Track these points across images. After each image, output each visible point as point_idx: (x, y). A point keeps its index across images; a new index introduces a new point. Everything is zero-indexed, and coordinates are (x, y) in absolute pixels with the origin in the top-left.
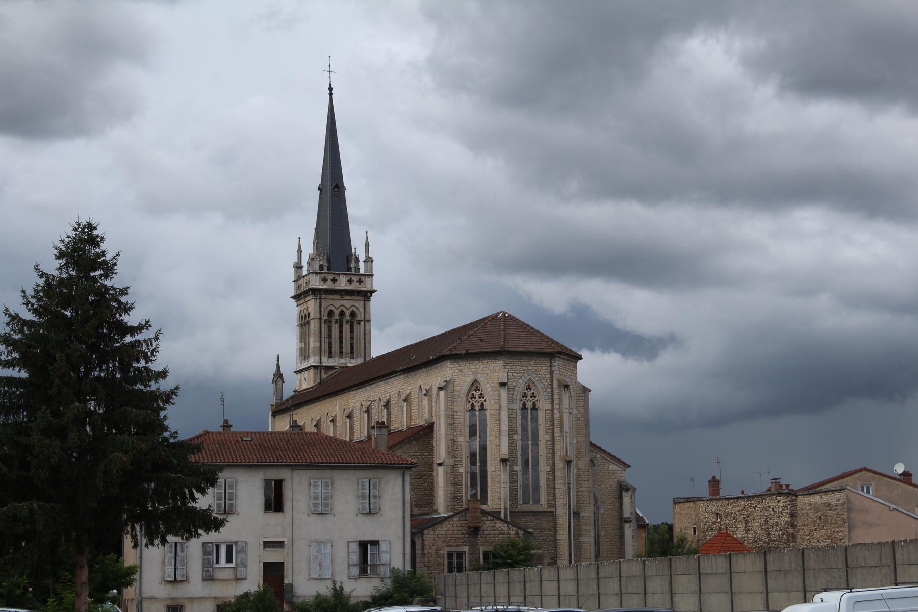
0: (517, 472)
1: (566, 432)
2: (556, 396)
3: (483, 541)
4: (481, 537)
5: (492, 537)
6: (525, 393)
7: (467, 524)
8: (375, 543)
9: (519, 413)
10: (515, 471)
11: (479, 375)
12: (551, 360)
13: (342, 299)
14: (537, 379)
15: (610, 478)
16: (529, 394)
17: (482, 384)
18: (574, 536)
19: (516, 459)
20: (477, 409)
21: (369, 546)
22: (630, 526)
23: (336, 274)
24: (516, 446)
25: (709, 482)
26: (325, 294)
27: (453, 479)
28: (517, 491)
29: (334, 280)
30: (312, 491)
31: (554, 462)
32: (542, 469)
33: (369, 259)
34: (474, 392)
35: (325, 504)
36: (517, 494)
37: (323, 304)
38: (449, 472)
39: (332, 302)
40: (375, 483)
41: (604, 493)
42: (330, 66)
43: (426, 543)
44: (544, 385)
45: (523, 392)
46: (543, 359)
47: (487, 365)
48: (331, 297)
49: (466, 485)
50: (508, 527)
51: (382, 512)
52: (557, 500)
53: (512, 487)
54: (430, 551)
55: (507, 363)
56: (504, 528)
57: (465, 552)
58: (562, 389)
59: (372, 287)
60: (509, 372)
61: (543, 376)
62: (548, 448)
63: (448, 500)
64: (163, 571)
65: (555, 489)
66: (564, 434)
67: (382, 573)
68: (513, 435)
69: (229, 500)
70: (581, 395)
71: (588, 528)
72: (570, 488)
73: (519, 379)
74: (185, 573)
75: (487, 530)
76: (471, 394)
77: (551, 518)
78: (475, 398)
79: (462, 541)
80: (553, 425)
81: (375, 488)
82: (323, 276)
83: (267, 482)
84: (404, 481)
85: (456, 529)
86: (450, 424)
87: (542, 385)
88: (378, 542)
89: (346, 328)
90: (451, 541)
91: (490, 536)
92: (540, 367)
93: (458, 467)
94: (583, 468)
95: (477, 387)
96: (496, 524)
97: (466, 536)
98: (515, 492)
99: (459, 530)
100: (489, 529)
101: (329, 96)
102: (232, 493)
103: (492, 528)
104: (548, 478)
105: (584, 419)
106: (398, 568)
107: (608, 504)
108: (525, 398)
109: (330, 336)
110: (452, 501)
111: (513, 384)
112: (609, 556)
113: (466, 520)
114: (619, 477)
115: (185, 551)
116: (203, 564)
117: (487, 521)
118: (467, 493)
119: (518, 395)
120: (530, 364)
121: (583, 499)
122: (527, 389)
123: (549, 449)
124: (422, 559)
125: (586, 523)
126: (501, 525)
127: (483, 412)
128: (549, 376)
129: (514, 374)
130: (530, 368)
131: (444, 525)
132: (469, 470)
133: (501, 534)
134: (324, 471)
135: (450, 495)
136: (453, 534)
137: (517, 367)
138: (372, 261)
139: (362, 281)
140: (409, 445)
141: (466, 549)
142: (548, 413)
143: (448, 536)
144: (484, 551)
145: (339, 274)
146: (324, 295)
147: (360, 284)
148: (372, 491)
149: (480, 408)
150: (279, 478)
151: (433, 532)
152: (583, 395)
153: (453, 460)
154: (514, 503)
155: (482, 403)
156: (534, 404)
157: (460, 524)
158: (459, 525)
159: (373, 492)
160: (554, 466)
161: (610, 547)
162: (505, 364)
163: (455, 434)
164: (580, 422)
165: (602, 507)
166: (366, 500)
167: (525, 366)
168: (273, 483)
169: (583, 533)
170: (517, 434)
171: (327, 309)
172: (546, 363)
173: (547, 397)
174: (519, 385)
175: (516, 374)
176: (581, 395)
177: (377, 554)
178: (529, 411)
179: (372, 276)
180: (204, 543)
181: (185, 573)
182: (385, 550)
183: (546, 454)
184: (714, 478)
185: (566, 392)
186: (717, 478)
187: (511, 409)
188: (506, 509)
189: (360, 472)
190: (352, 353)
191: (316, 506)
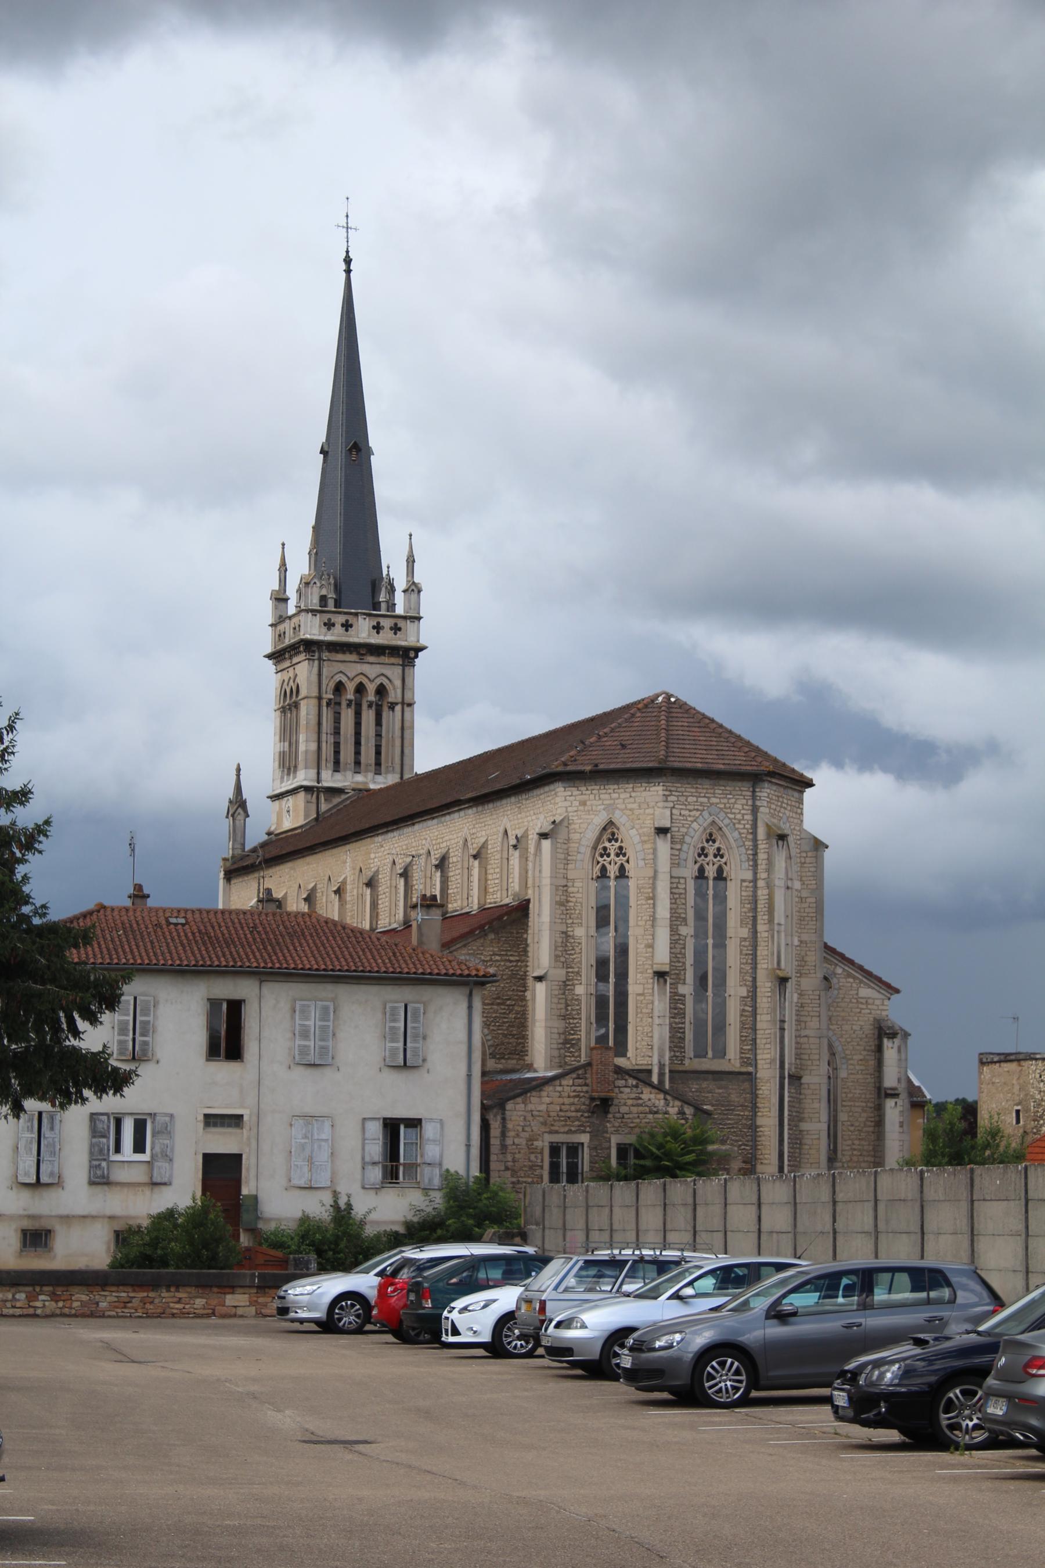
0: (684, 996)
1: (779, 924)
2: (762, 856)
3: (617, 1124)
4: (614, 1117)
5: (635, 1118)
6: (616, 840)
7: (587, 1092)
8: (415, 1123)
10: (681, 995)
11: (617, 812)
13: (361, 661)
14: (727, 821)
15: (860, 1012)
16: (711, 849)
17: (622, 828)
19: (682, 973)
20: (612, 876)
21: (402, 1127)
22: (896, 1103)
23: (351, 614)
24: (684, 948)
26: (330, 651)
28: (684, 1033)
29: (347, 626)
30: (298, 1022)
31: (754, 979)
32: (732, 993)
33: (413, 587)
34: (607, 844)
35: (322, 1047)
36: (684, 1039)
37: (325, 671)
39: (342, 667)
40: (416, 1011)
41: (849, 1040)
42: (347, 216)
43: (510, 1125)
44: (740, 834)
46: (740, 784)
47: (633, 794)
48: (340, 657)
49: (588, 1018)
50: (665, 1099)
51: (428, 1065)
52: (758, 1051)
53: (674, 1025)
55: (670, 791)
56: (657, 1102)
57: (582, 1144)
58: (775, 841)
59: (418, 641)
60: (674, 807)
61: (739, 816)
62: (744, 952)
63: (552, 1046)
64: (16, 1163)
66: (776, 928)
68: (680, 927)
69: (143, 1035)
72: (784, 1029)
73: (692, 822)
74: (56, 1170)
75: (625, 1104)
76: (600, 847)
77: (746, 1085)
78: (608, 855)
79: (577, 1123)
80: (755, 909)
81: (416, 1020)
82: (326, 617)
83: (214, 1004)
84: (470, 1007)
85: (567, 1101)
87: (736, 834)
89: (368, 717)
90: (556, 1123)
91: (631, 1116)
92: (733, 801)
93: (573, 985)
94: (811, 992)
95: (613, 834)
96: (642, 1093)
97: (586, 1115)
98: (679, 1035)
99: (573, 1104)
100: (630, 1102)
101: (344, 275)
102: (149, 1022)
103: (635, 1102)
104: (744, 1010)
105: (813, 900)
106: (456, 1172)
107: (855, 1062)
109: (337, 732)
110: (559, 1049)
111: (682, 830)
112: (855, 1159)
113: (586, 1085)
114: (878, 1012)
115: (57, 1127)
116: (91, 1153)
117: (626, 1087)
118: (588, 1033)
119: (690, 852)
120: (714, 793)
121: (809, 1051)
123: (746, 955)
124: (501, 1156)
125: (814, 1097)
126: (652, 1096)
127: (623, 881)
128: (749, 817)
129: (683, 812)
130: (714, 800)
131: (544, 1094)
132: (593, 991)
133: (651, 1112)
134: (321, 986)
135: (556, 1036)
137: (690, 799)
138: (419, 591)
139: (400, 629)
140: (482, 941)
141: (584, 1138)
142: (747, 887)
143: (552, 1114)
144: (618, 1144)
145: (356, 614)
146: (327, 654)
147: (395, 634)
149: (716, 875)
150: (236, 996)
151: (523, 1106)
153: (563, 972)
154: (678, 1054)
155: (622, 865)
156: (720, 870)
157: (574, 1091)
158: (572, 1094)
159: (414, 1028)
160: (755, 987)
161: (857, 1142)
162: (667, 793)
163: (569, 921)
164: (806, 905)
165: (844, 1066)
166: (398, 1042)
167: (705, 797)
168: (225, 1006)
169: (806, 1115)
170: (686, 925)
171: (332, 681)
172: (744, 793)
173: (744, 858)
175: (687, 813)
176: (810, 854)
177: (418, 1144)
178: (711, 882)
179: (419, 618)
180: (92, 1114)
181: (56, 1170)
183: (741, 963)
185: (780, 848)
187: (675, 878)
188: (661, 1066)
189: (389, 988)
190: (378, 764)
191: (304, 1051)
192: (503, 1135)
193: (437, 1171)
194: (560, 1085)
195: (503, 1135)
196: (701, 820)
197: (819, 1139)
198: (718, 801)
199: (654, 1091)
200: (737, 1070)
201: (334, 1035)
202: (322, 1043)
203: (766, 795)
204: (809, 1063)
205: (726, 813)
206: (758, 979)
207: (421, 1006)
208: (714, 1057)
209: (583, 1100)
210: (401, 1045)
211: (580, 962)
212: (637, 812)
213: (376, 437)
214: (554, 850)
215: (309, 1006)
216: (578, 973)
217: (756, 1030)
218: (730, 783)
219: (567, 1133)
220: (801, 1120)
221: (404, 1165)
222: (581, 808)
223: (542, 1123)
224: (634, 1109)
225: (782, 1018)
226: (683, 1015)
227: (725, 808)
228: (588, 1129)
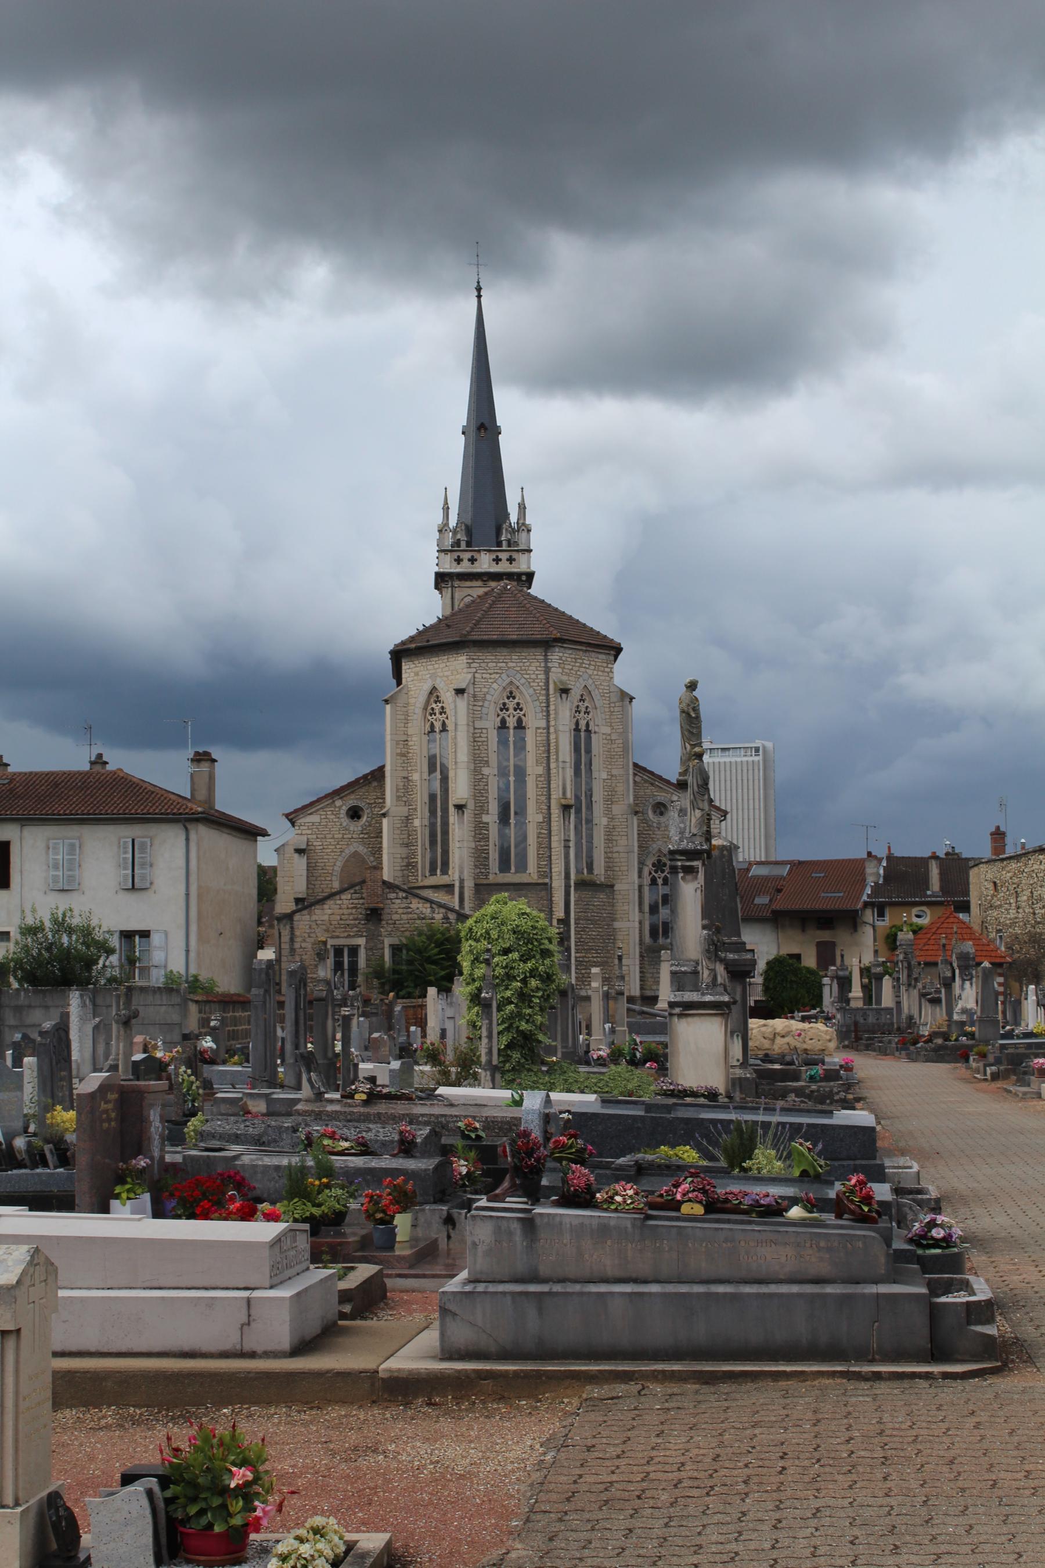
2: (552, 707)
3: (390, 929)
6: (504, 704)
7: (363, 904)
8: (145, 934)
9: (493, 737)
10: (485, 823)
11: (438, 678)
12: (546, 652)
14: (523, 681)
16: (511, 704)
18: (576, 920)
24: (487, 785)
25: (992, 834)
26: (460, 580)
27: (406, 836)
28: (488, 853)
29: (472, 560)
30: (51, 856)
31: (549, 807)
34: (434, 706)
35: (70, 876)
36: (488, 858)
38: (399, 826)
43: (297, 933)
44: (535, 690)
45: (502, 701)
47: (448, 664)
48: (468, 584)
49: (423, 845)
50: (431, 907)
52: (553, 866)
54: (304, 945)
56: (424, 910)
58: (558, 695)
59: (529, 568)
61: (533, 676)
63: (396, 868)
65: (550, 848)
66: (561, 765)
67: (154, 980)
70: (617, 704)
71: (626, 908)
72: (569, 847)
75: (396, 913)
76: (429, 708)
77: (543, 893)
78: (507, 710)
79: (355, 929)
80: (548, 751)
82: (455, 555)
84: (187, 839)
85: (346, 912)
86: (403, 755)
87: (531, 691)
88: (149, 931)
91: (402, 922)
92: (528, 664)
94: (620, 816)
95: (438, 697)
97: (363, 922)
100: (400, 911)
101: (476, 299)
104: (540, 833)
106: (178, 972)
108: (518, 711)
113: (362, 898)
118: (423, 857)
121: (619, 864)
122: (508, 698)
123: (542, 788)
124: (290, 958)
125: (623, 901)
126: (420, 905)
127: (443, 734)
128: (542, 676)
129: (484, 676)
130: (511, 664)
131: (326, 906)
132: (427, 823)
133: (419, 918)
135: (399, 860)
136: (341, 919)
137: (490, 665)
138: (529, 531)
141: (361, 941)
142: (541, 733)
143: (333, 922)
144: (390, 945)
145: (479, 551)
146: (458, 582)
147: (511, 563)
148: (137, 855)
149: (516, 725)
151: (308, 917)
152: (620, 704)
153: (406, 809)
154: (483, 871)
156: (520, 721)
160: (550, 814)
164: (615, 746)
169: (618, 916)
170: (488, 766)
173: (538, 709)
174: (492, 692)
175: (488, 676)
176: (617, 704)
178: (512, 731)
179: (531, 551)
182: (158, 945)
184: (998, 828)
186: (1002, 829)
188: (462, 881)
189: (123, 827)
191: (55, 879)
192: (292, 940)
193: (163, 972)
194: (340, 899)
195: (292, 940)
196: (500, 681)
197: (628, 935)
198: (514, 664)
199: (421, 901)
200: (534, 882)
201: (80, 866)
202: (70, 873)
203: (557, 657)
204: (620, 873)
205: (522, 674)
206: (552, 808)
207: (148, 840)
208: (516, 872)
209: (359, 910)
210: (130, 872)
211: (416, 801)
212: (450, 678)
213: (502, 418)
214: (394, 713)
215: (58, 844)
216: (415, 809)
217: (551, 848)
218: (525, 650)
219: (346, 937)
220: (614, 920)
221: (139, 967)
222: (416, 678)
223: (325, 930)
224: (404, 917)
225: (567, 838)
226: (487, 839)
227: (521, 670)
228: (365, 934)
